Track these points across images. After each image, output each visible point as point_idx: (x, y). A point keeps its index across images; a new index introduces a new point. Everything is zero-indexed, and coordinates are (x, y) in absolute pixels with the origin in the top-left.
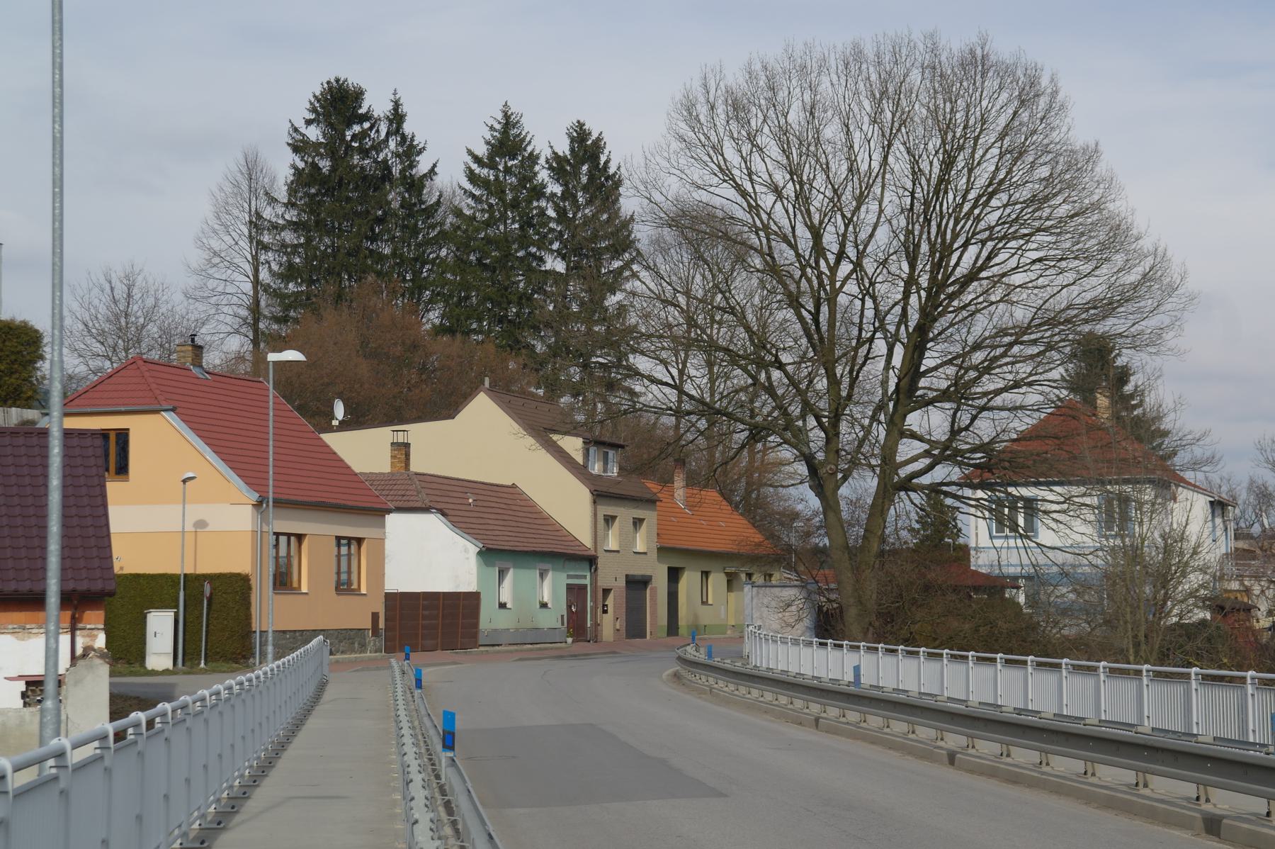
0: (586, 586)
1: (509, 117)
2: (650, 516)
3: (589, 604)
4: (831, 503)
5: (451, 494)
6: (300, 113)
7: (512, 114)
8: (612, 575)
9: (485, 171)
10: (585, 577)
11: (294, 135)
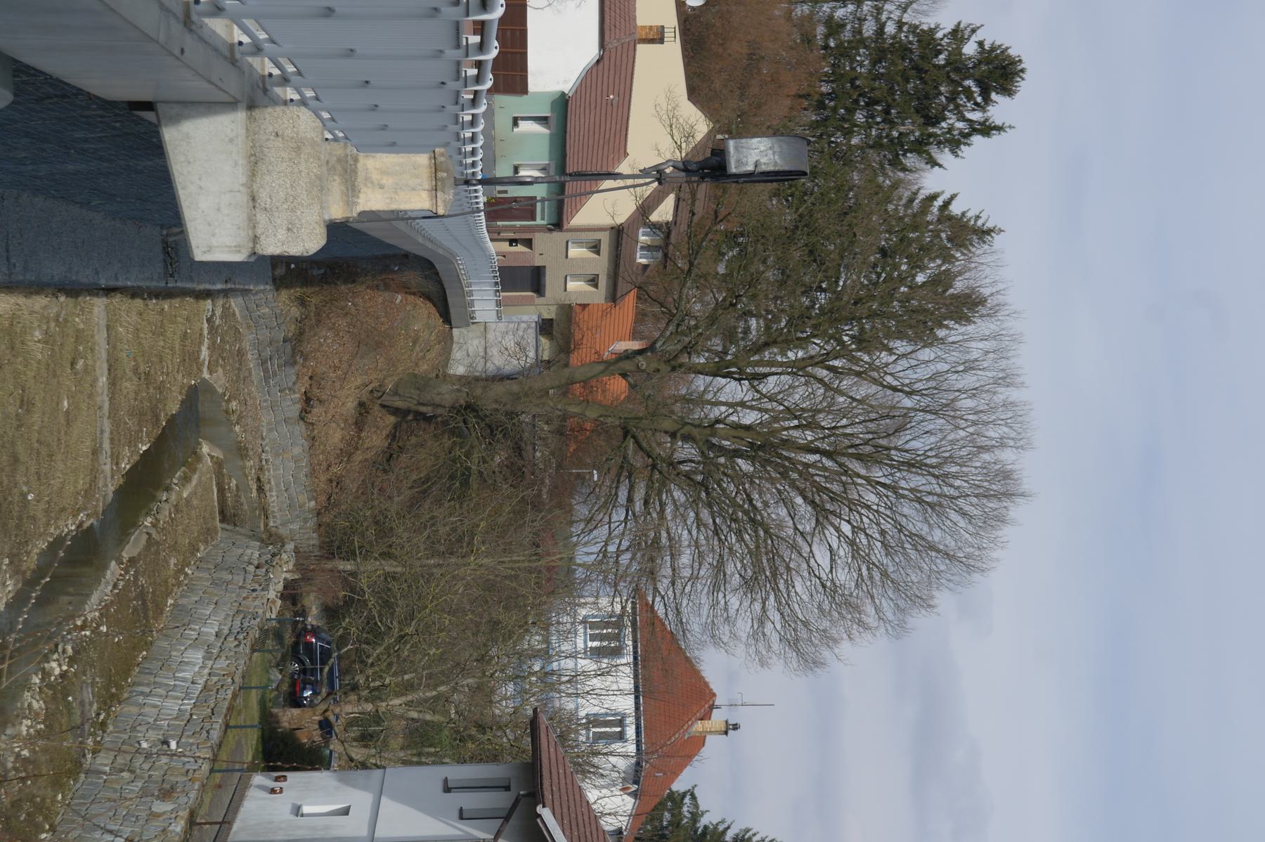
0: (534, 219)
1: (989, 234)
2: (598, 296)
3: (518, 223)
4: (612, 368)
5: (617, 77)
6: (989, 36)
7: (992, 237)
8: (546, 249)
9: (935, 210)
10: (543, 219)
11: (969, 29)
